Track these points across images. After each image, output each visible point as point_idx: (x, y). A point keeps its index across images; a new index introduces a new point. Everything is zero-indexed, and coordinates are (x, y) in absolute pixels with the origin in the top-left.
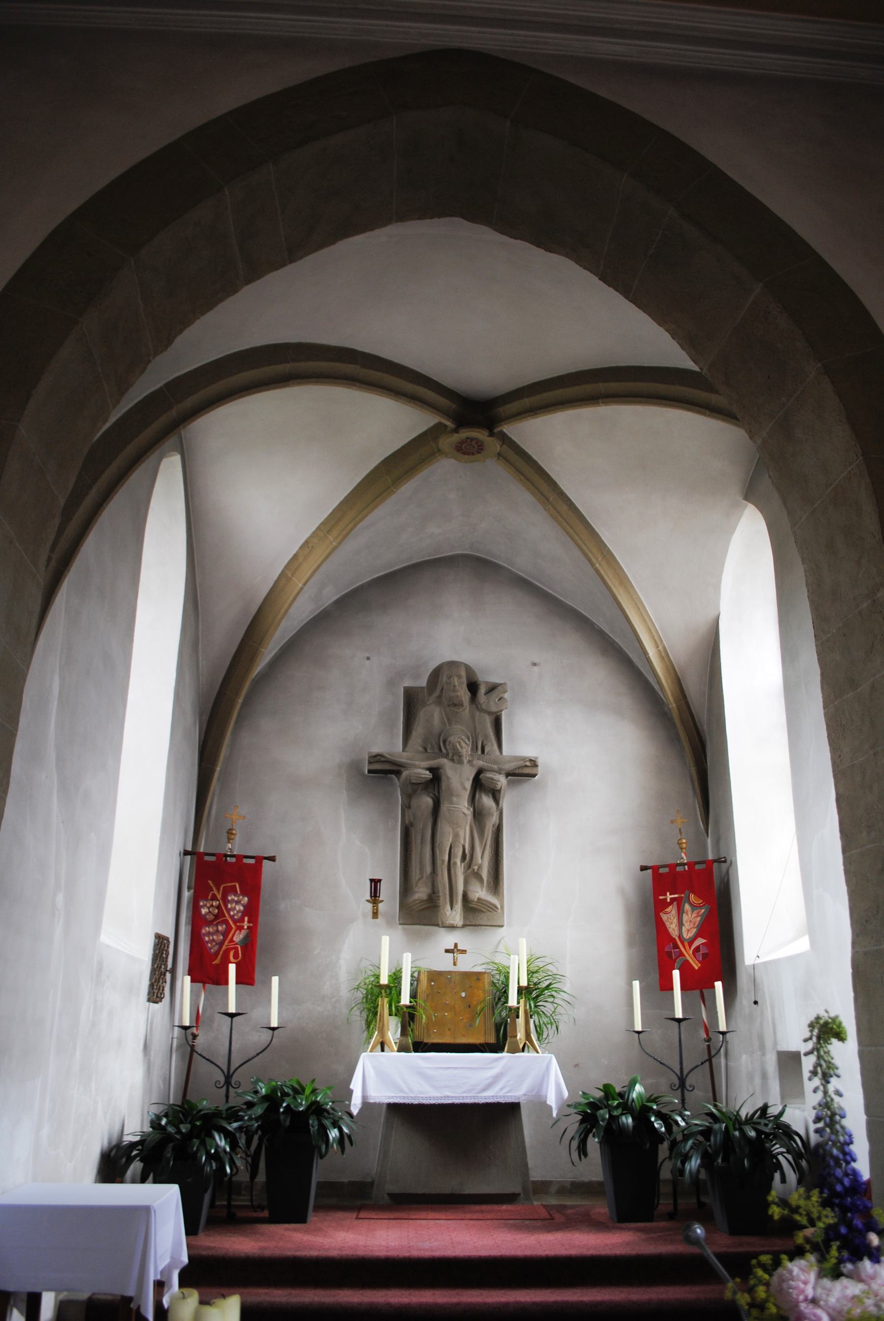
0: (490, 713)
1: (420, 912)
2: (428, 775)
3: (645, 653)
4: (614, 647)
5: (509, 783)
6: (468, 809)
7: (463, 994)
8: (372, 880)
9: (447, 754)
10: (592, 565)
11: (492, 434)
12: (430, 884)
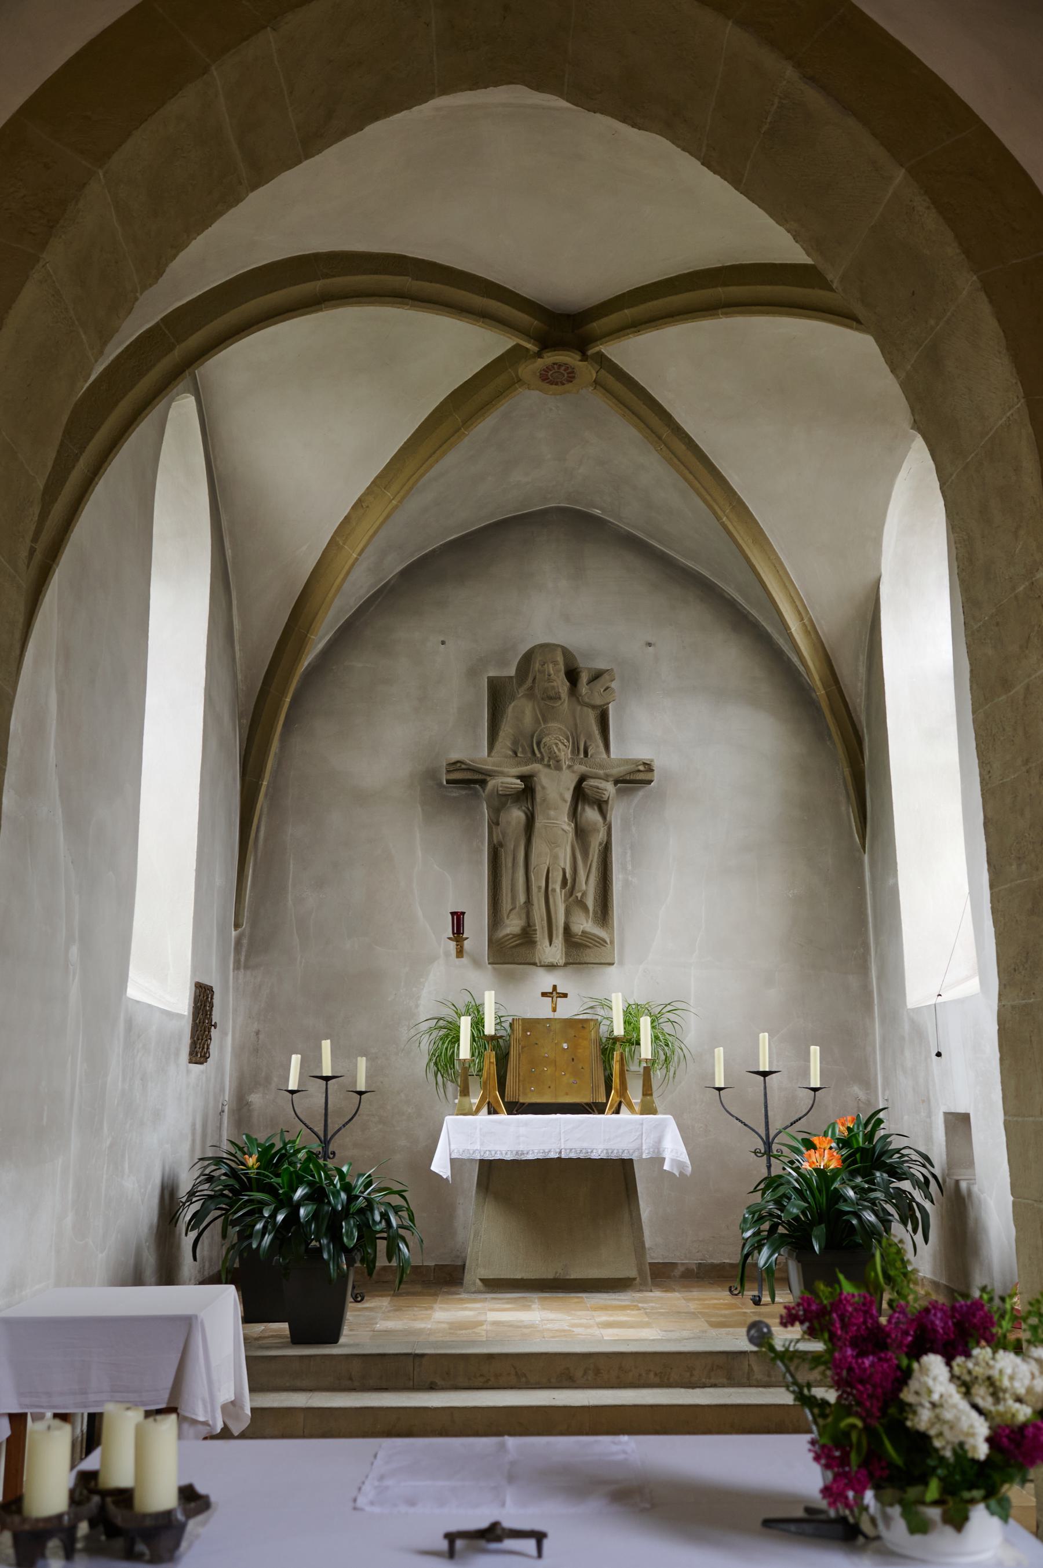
0: (594, 707)
1: (512, 952)
2: (519, 784)
3: (786, 627)
4: (745, 620)
5: (619, 792)
6: (569, 825)
7: (565, 1046)
8: (453, 914)
9: (542, 759)
10: (718, 519)
11: (584, 357)
12: (524, 916)
